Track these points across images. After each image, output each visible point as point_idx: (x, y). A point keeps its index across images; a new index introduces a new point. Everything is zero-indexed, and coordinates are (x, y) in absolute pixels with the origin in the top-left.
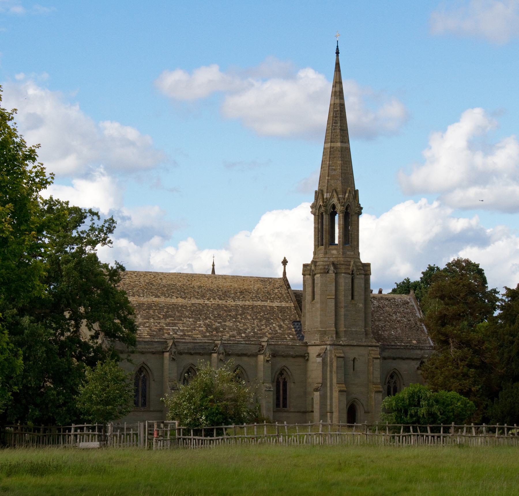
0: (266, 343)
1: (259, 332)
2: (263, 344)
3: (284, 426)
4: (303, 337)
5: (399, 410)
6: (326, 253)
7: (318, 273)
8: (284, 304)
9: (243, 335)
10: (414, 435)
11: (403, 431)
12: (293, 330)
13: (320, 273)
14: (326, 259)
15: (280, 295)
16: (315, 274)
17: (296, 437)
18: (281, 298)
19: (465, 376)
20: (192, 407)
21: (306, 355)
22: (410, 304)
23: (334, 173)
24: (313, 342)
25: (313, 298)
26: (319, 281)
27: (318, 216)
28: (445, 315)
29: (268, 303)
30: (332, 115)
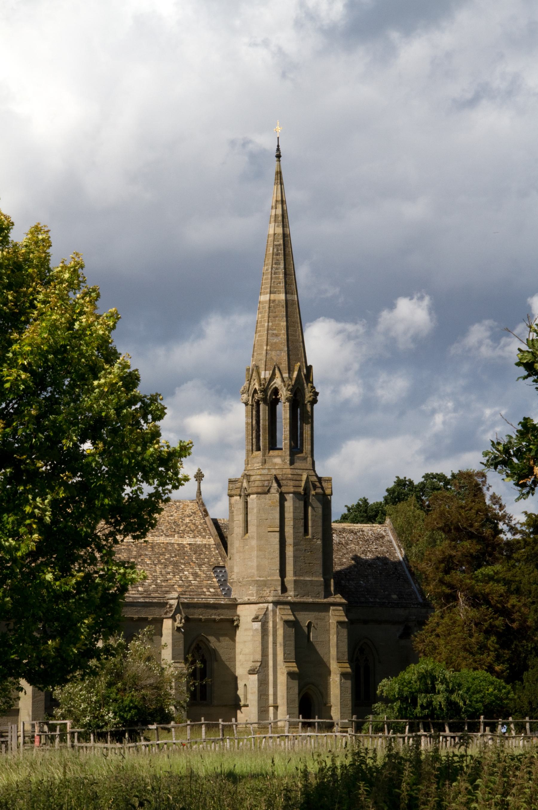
0: (177, 601)
1: (163, 584)
2: (172, 602)
3: (232, 725)
4: (229, 590)
5: (403, 699)
6: (264, 462)
7: (253, 494)
8: (199, 541)
9: (140, 589)
10: (426, 736)
11: (409, 730)
12: (215, 580)
13: (257, 493)
14: (265, 472)
15: (193, 527)
16: (249, 495)
17: (250, 741)
18: (195, 531)
19: (483, 648)
20: (94, 699)
21: (235, 618)
22: (386, 539)
23: (275, 340)
24: (246, 599)
25: (246, 531)
26: (255, 505)
27: (252, 405)
28: (451, 557)
29: (175, 539)
30: (271, 252)
